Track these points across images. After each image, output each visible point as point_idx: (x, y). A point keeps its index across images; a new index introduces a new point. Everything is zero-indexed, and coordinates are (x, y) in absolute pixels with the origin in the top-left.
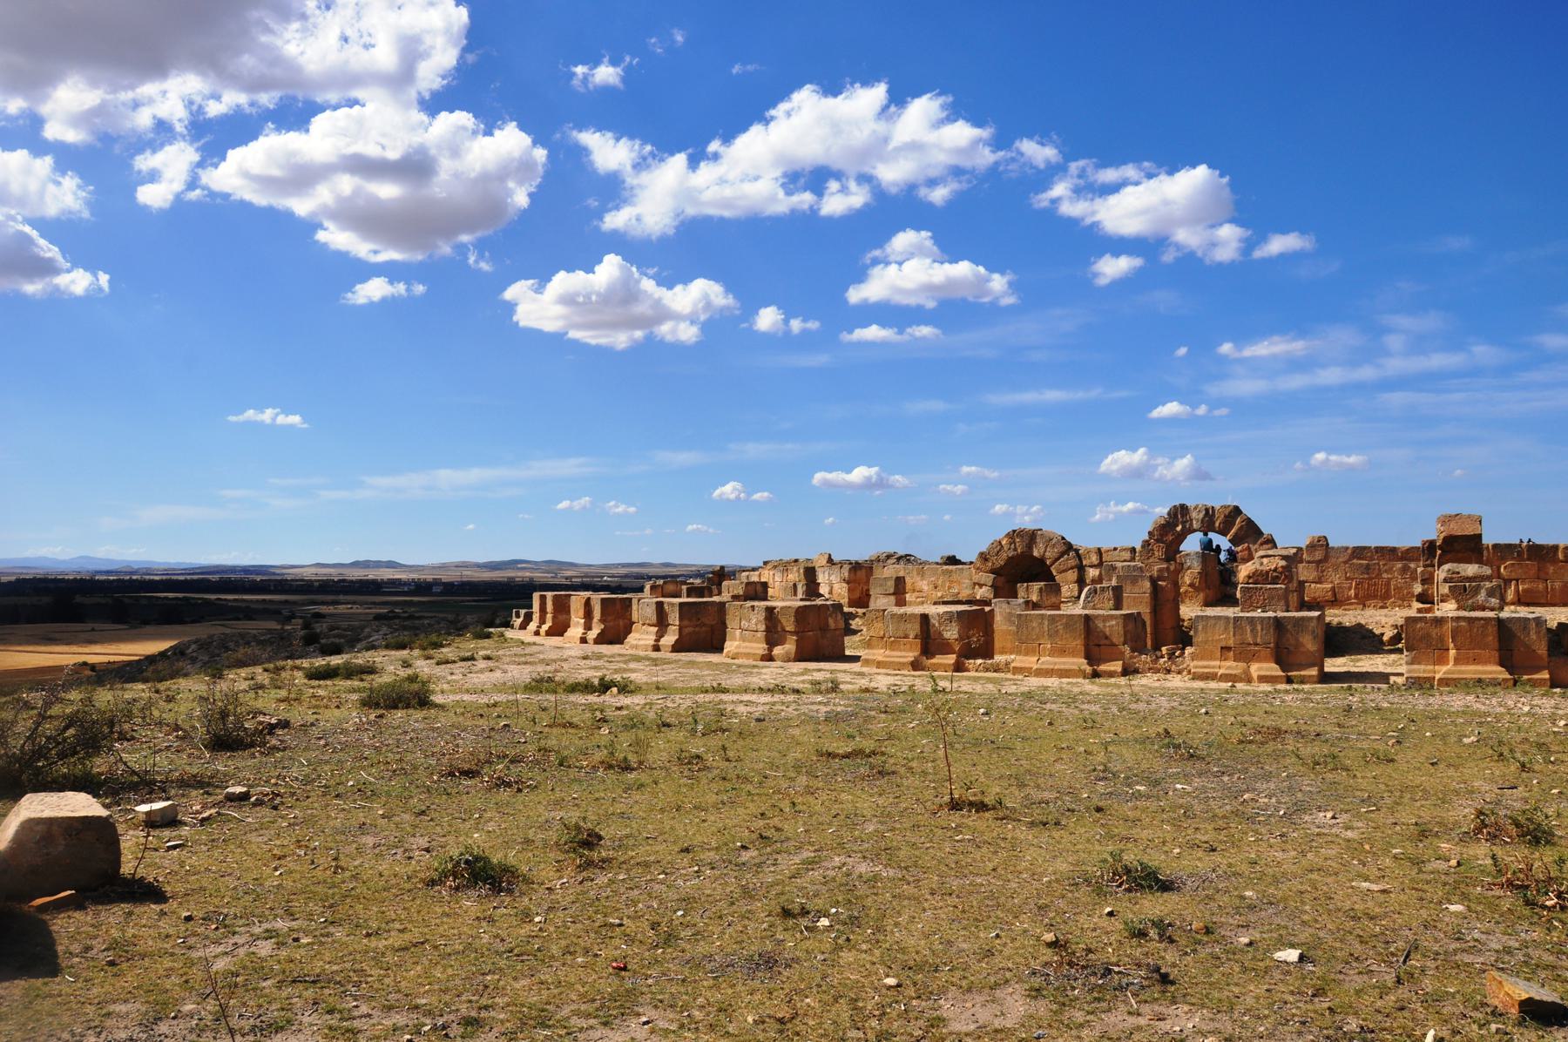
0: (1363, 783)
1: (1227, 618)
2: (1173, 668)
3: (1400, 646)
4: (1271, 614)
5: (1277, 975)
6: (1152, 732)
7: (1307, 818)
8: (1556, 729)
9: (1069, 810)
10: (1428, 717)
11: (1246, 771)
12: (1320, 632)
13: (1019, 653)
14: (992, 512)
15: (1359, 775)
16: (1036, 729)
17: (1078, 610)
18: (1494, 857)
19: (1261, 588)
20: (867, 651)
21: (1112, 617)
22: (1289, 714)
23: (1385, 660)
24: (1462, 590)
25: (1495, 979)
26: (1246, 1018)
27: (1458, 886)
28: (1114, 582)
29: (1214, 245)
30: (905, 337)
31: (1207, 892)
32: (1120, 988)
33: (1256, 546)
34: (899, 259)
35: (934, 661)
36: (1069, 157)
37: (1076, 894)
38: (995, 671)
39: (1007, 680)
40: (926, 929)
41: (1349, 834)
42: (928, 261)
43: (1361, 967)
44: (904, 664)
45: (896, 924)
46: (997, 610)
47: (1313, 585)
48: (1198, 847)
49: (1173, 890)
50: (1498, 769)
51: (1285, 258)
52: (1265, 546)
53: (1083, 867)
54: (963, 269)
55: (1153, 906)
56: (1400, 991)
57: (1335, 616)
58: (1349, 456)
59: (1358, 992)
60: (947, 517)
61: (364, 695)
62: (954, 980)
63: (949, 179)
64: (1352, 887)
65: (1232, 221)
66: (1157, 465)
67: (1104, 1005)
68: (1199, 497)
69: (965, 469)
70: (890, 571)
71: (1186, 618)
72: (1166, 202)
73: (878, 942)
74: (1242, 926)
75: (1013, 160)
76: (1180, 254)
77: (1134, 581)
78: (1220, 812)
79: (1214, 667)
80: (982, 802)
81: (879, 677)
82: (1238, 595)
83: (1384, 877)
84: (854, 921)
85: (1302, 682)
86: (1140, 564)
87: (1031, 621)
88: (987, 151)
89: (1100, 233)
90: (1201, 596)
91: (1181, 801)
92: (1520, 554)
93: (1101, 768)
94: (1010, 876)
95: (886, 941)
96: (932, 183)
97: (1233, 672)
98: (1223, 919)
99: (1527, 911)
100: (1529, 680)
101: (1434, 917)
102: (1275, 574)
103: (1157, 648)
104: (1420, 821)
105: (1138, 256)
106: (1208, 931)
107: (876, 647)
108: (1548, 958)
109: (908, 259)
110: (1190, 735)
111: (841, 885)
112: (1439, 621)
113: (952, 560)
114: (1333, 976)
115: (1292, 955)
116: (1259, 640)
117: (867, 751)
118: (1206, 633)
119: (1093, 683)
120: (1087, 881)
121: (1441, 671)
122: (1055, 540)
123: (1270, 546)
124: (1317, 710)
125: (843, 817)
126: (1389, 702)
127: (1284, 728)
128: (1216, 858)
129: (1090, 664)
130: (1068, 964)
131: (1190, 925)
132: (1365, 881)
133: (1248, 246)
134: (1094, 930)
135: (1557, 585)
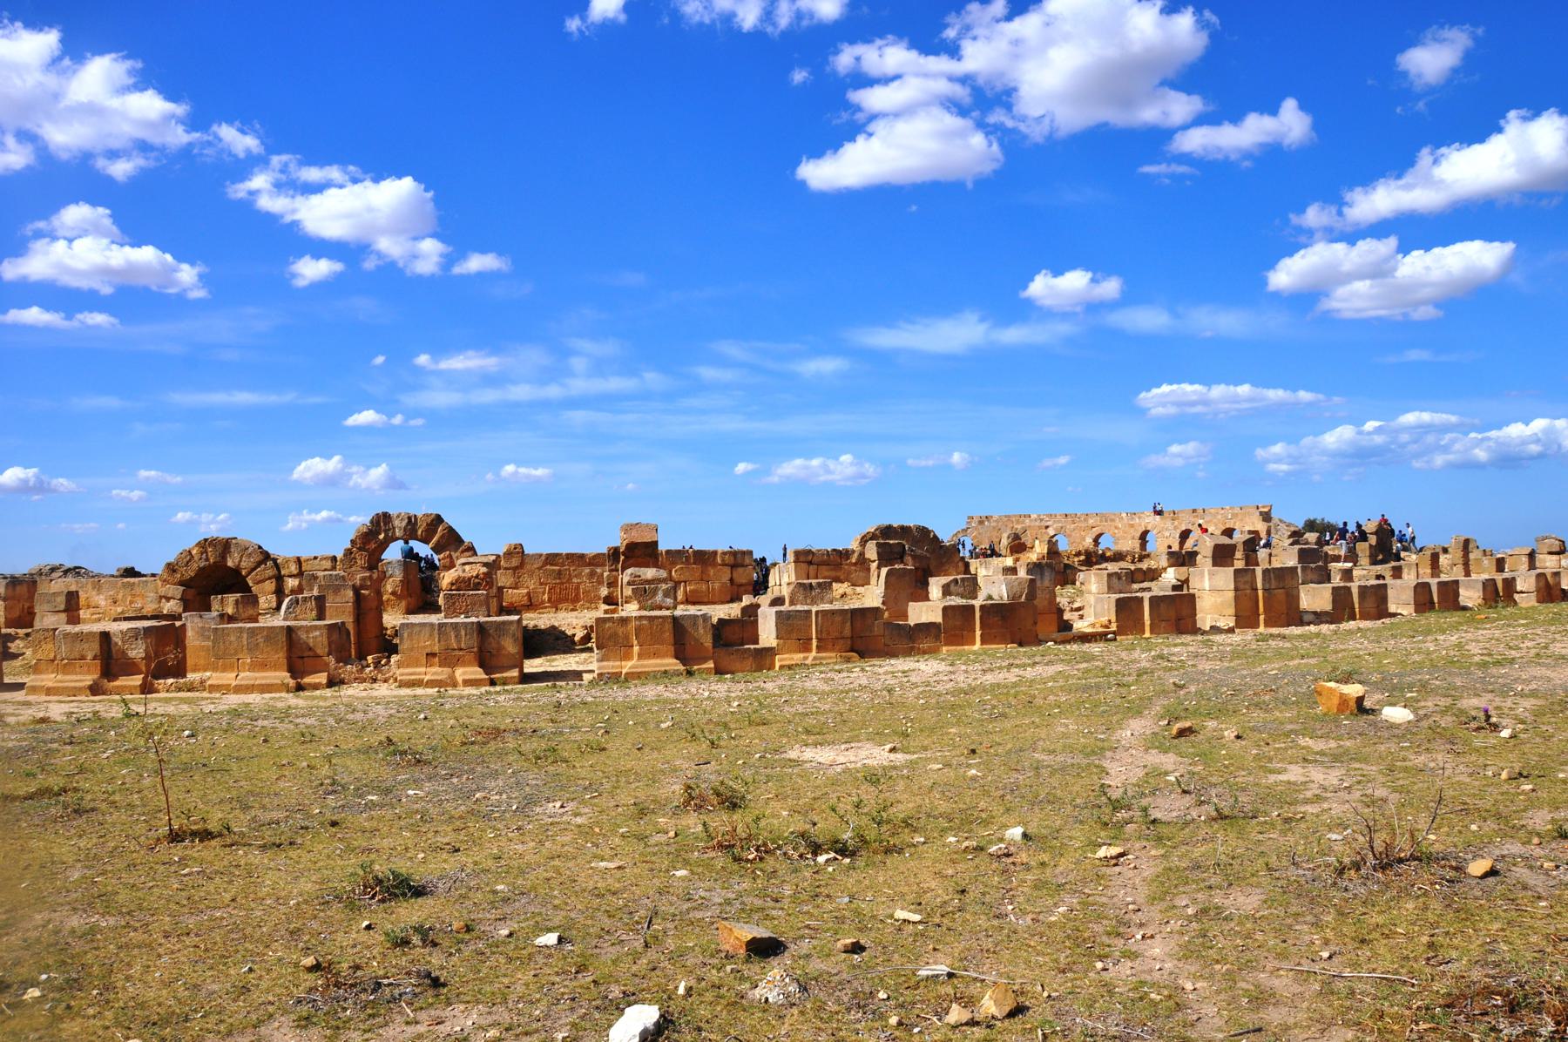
0: (583, 773)
1: (432, 625)
2: (379, 676)
3: (590, 645)
4: (473, 619)
5: (540, 960)
6: (374, 740)
7: (538, 810)
8: (732, 710)
9: (302, 828)
10: (628, 707)
11: (473, 771)
12: (519, 635)
13: (215, 669)
14: (173, 520)
15: (577, 765)
16: (250, 748)
17: (278, 621)
18: (704, 824)
19: (464, 595)
20: (32, 677)
21: (316, 628)
22: (505, 714)
23: (577, 659)
24: (643, 592)
25: (726, 927)
26: (520, 1006)
27: (679, 856)
28: (315, 592)
29: (415, 256)
30: (75, 324)
31: (460, 892)
32: (394, 1000)
33: (458, 554)
34: (69, 234)
35: (117, 683)
36: (271, 149)
37: (328, 913)
38: (189, 690)
39: (203, 699)
40: (165, 977)
41: (579, 820)
42: (105, 241)
43: (613, 939)
44: (80, 689)
45: (128, 978)
46: (189, 625)
47: (510, 591)
48: (441, 849)
49: (426, 894)
50: (693, 748)
51: (481, 276)
52: (467, 554)
53: (330, 885)
54: (147, 254)
55: (410, 913)
56: (649, 954)
57: (532, 619)
58: (536, 469)
59: (614, 962)
60: (121, 526)
61: (1540, 702)
62: (209, 1026)
63: (135, 153)
64: (592, 868)
65: (434, 235)
66: (352, 474)
67: (380, 1020)
68: (401, 505)
69: (144, 473)
70: (59, 585)
71: (389, 626)
72: (370, 209)
73: (108, 1002)
74: (500, 919)
75: (209, 143)
76: (381, 263)
77: (337, 590)
78: (456, 813)
79: (419, 674)
80: (206, 830)
81: (51, 705)
82: (441, 601)
83: (616, 855)
84: (73, 985)
85: (504, 684)
86: (342, 573)
87: (228, 635)
88: (180, 129)
89: (300, 233)
90: (404, 603)
91: (416, 806)
92: (687, 558)
93: (328, 781)
94: (253, 905)
95: (118, 1000)
96: (113, 155)
97: (439, 678)
98: (480, 916)
99: (736, 867)
100: (699, 669)
101: (666, 884)
102: (477, 580)
103: (361, 657)
104: (637, 801)
105: (339, 261)
106: (468, 929)
107: (46, 671)
108: (758, 903)
109: (80, 237)
110: (413, 741)
111: (50, 945)
112: (624, 621)
113: (131, 572)
114: (590, 952)
115: (551, 939)
116: (463, 646)
117: (56, 788)
118: (412, 640)
119: (298, 697)
120: (338, 898)
121: (627, 666)
122: (251, 550)
123: (470, 553)
124: (530, 708)
125: (37, 867)
126: (592, 696)
127: (502, 727)
128: (461, 857)
129: (293, 677)
130: (335, 985)
131: (450, 925)
132: (602, 861)
133: (448, 261)
134: (354, 946)
135: (717, 585)
